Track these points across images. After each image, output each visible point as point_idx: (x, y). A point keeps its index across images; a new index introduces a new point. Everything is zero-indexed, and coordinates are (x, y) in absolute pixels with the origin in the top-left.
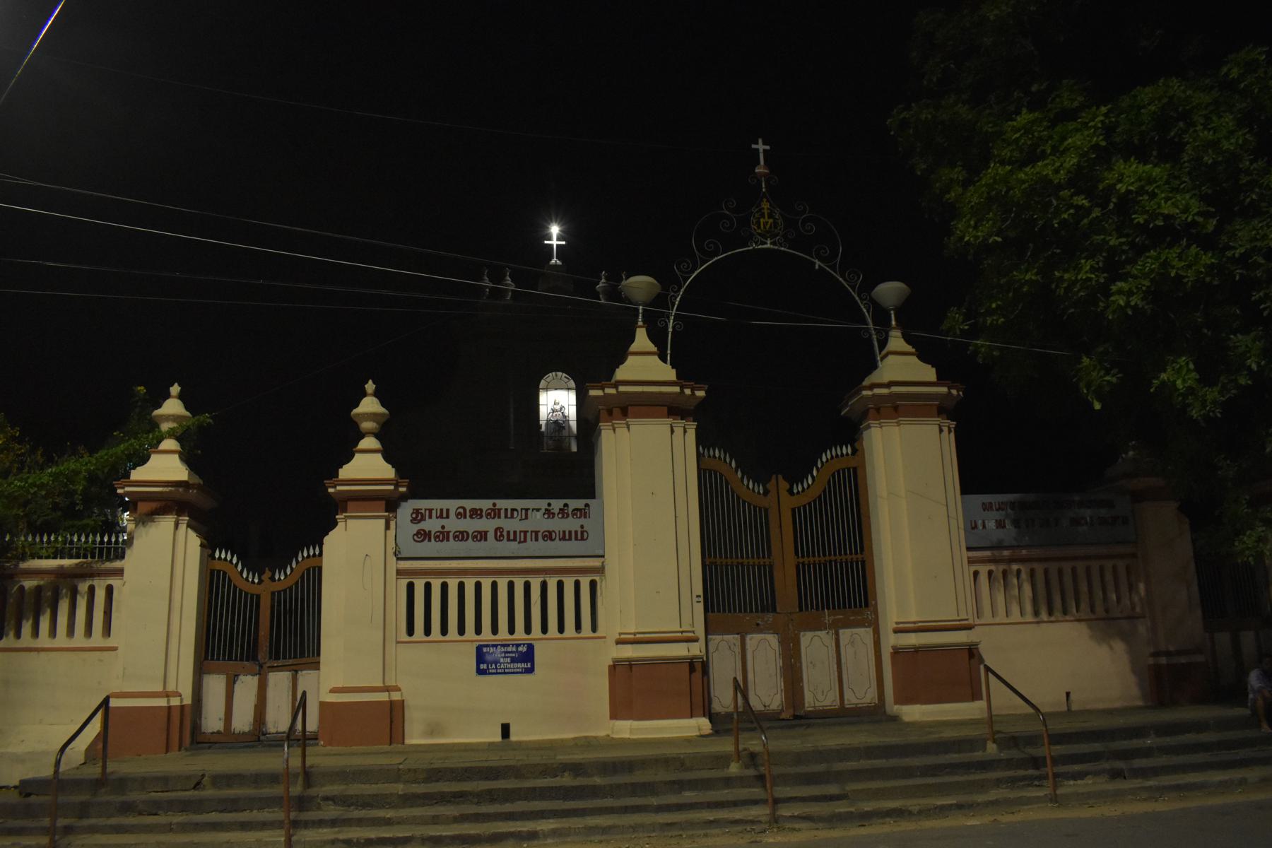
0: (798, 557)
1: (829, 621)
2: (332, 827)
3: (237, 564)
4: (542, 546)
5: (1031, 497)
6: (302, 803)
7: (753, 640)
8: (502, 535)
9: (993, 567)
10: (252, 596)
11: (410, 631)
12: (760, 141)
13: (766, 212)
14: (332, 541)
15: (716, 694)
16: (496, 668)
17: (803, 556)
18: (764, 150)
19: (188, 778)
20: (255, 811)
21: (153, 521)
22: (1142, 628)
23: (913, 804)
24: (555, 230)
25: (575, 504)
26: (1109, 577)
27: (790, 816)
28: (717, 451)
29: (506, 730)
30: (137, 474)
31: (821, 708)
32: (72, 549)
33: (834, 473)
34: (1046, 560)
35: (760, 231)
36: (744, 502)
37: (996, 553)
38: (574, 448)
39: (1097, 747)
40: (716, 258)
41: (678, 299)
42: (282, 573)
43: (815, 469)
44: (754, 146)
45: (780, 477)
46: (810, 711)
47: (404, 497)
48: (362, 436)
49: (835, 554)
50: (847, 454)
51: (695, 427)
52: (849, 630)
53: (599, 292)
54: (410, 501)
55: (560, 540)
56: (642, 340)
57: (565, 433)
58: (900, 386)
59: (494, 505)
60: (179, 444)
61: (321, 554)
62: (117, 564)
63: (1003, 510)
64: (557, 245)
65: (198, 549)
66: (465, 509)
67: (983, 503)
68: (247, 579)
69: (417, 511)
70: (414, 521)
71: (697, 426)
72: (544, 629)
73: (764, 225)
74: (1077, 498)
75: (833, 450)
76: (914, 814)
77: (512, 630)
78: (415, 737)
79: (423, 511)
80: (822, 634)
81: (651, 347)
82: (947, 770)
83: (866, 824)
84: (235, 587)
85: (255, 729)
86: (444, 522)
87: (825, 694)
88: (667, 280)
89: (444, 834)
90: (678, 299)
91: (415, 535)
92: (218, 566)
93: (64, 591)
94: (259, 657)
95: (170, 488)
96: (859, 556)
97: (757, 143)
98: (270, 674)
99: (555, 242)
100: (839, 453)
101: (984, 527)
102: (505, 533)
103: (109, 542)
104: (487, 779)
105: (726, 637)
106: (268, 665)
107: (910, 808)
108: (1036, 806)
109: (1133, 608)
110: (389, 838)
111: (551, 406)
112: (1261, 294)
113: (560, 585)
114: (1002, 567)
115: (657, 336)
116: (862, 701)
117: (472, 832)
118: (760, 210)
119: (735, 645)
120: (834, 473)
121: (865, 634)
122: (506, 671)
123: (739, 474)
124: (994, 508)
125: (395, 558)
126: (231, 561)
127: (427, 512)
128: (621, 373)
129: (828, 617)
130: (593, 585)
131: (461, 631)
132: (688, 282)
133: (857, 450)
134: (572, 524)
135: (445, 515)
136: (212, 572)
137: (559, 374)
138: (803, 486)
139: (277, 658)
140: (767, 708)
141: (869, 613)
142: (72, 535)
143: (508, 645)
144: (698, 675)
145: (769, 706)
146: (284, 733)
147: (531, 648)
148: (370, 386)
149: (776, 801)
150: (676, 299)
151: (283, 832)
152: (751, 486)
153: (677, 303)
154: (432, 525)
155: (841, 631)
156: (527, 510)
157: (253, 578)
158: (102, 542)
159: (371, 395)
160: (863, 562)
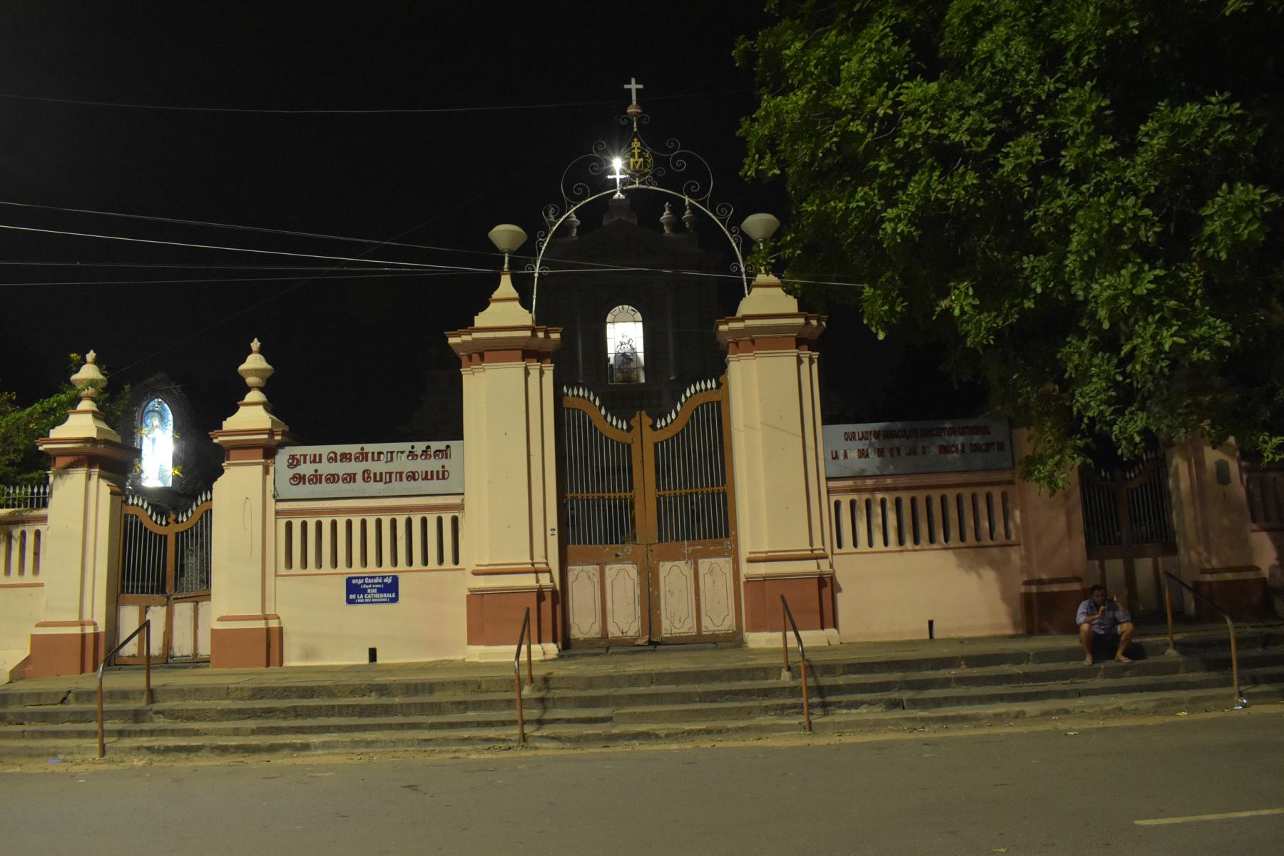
0: (659, 490)
2: (151, 736)
5: (898, 425)
6: (137, 716)
7: (612, 570)
8: (369, 477)
9: (855, 496)
10: (161, 536)
11: (289, 563)
12: (633, 80)
14: (220, 485)
16: (364, 598)
18: (637, 90)
19: (56, 694)
21: (68, 474)
23: (661, 728)
24: (617, 163)
25: (440, 445)
26: (982, 505)
28: (581, 390)
29: (373, 654)
30: (55, 433)
32: (8, 499)
34: (895, 489)
36: (607, 438)
37: (859, 482)
38: (643, 380)
39: (896, 676)
40: (584, 202)
41: (545, 245)
44: (626, 86)
45: (644, 413)
46: (666, 638)
47: (282, 445)
49: (697, 487)
50: (712, 388)
51: (552, 368)
52: (709, 560)
53: (663, 224)
54: (286, 448)
56: (506, 287)
57: (633, 365)
59: (362, 449)
61: (211, 499)
62: (42, 512)
63: (867, 439)
64: (621, 179)
65: (109, 496)
68: (156, 522)
69: (293, 457)
70: (291, 466)
71: (554, 367)
72: (410, 562)
74: (947, 425)
75: (703, 383)
76: (661, 738)
77: (380, 563)
78: (292, 660)
79: (298, 457)
80: (682, 563)
81: (515, 294)
82: (727, 696)
87: (682, 620)
88: (533, 226)
89: (230, 744)
90: (545, 245)
92: (130, 511)
94: (167, 590)
95: (80, 445)
96: (721, 488)
97: (630, 83)
99: (618, 177)
100: (703, 387)
101: (846, 456)
102: (372, 475)
103: (39, 493)
104: (304, 697)
106: (173, 597)
108: (788, 733)
109: (1008, 536)
111: (619, 339)
112: (1031, 213)
114: (865, 496)
115: (521, 285)
116: (720, 628)
117: (254, 743)
121: (724, 564)
122: (373, 600)
123: (603, 412)
125: (273, 501)
126: (142, 506)
127: (302, 457)
128: (481, 320)
129: (687, 547)
130: (455, 521)
131: (335, 563)
133: (722, 384)
134: (434, 465)
135: (317, 460)
136: (126, 516)
137: (626, 307)
138: (666, 421)
142: (9, 487)
143: (374, 577)
146: (188, 656)
147: (395, 579)
148: (255, 344)
151: (97, 740)
152: (614, 423)
153: (544, 248)
154: (306, 469)
155: (700, 561)
156: (392, 453)
157: (161, 521)
158: (33, 493)
159: (256, 352)
160: (725, 494)
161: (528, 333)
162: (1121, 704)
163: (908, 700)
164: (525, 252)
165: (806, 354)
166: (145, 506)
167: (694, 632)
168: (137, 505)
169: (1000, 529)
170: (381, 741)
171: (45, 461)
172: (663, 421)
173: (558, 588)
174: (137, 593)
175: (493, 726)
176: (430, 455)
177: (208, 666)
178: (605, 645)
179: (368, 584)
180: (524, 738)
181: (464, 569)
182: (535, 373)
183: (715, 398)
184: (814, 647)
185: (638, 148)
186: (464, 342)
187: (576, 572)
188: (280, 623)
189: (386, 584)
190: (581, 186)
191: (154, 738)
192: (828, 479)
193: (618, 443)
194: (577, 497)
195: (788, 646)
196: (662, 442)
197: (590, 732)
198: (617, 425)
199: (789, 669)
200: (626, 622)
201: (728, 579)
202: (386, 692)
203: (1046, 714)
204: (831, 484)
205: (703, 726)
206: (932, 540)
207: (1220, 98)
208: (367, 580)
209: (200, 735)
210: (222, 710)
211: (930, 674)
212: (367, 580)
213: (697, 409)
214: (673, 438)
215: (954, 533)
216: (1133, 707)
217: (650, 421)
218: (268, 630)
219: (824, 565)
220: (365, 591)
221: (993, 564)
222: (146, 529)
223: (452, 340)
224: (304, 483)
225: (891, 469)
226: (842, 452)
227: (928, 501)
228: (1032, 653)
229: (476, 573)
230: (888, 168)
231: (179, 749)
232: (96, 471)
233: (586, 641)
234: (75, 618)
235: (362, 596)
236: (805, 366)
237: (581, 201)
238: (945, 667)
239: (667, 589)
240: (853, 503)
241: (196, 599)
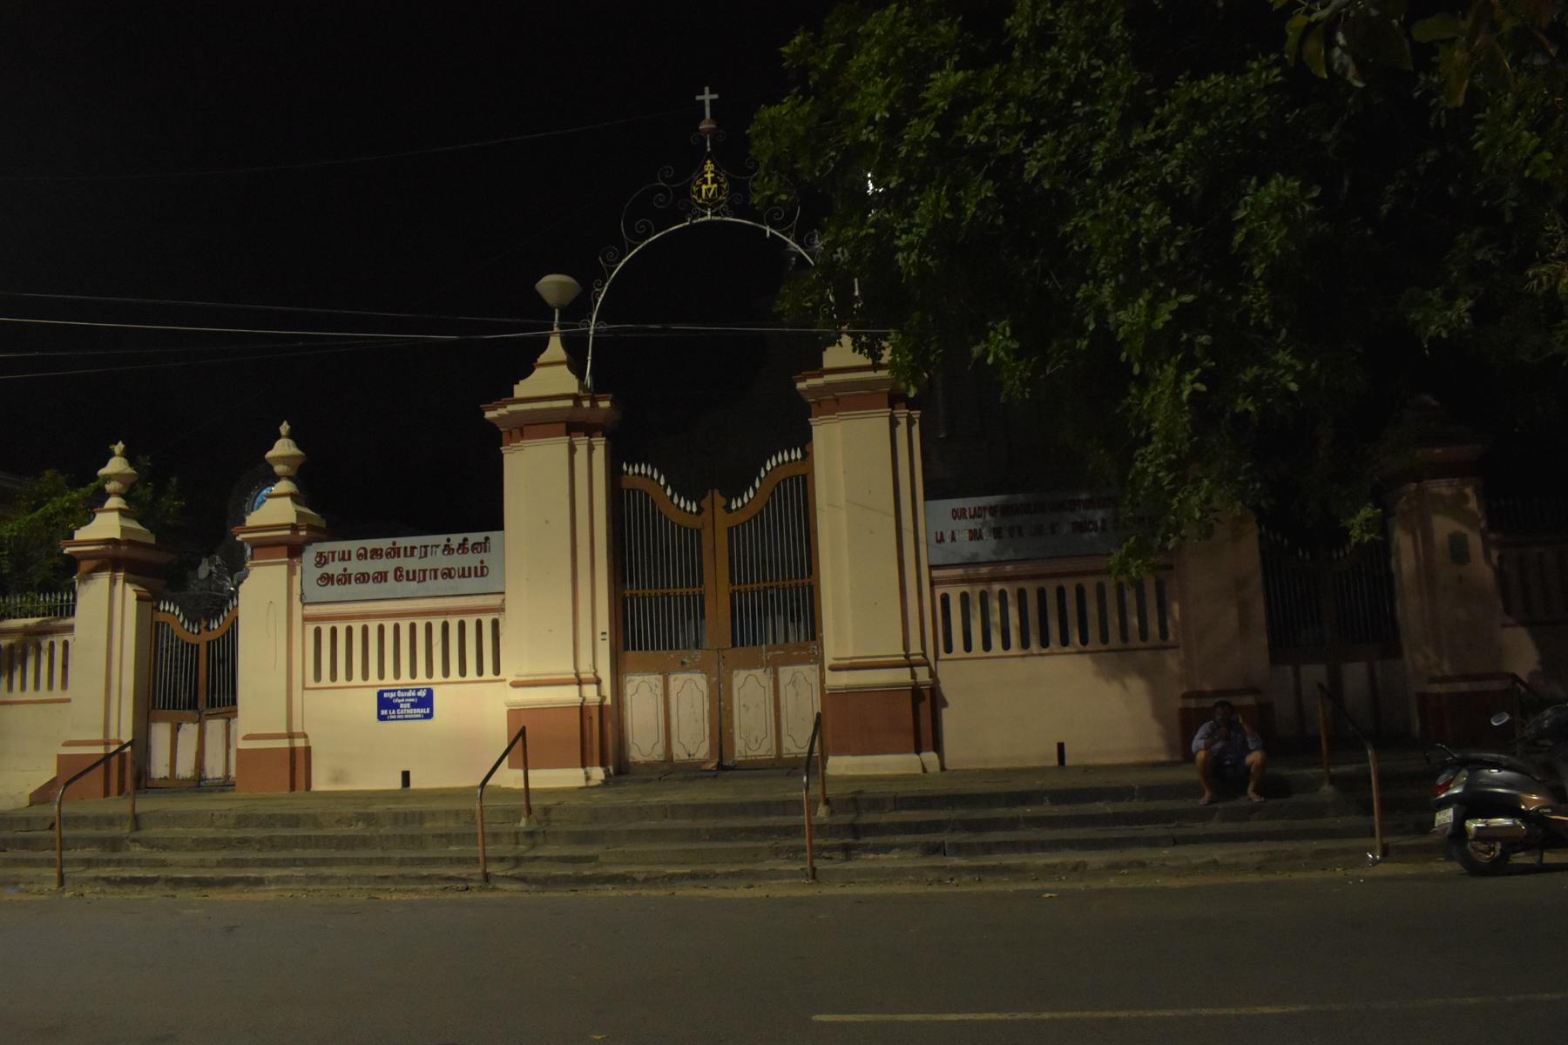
0: (733, 584)
1: (766, 657)
3: (179, 616)
4: (442, 584)
5: (1020, 498)
6: (115, 844)
7: (677, 680)
8: (401, 575)
9: (966, 588)
11: (318, 676)
12: (707, 89)
13: (709, 176)
15: (635, 741)
16: (396, 714)
17: (739, 583)
18: (711, 101)
19: (45, 819)
20: (79, 850)
21: (92, 579)
22: (1172, 661)
25: (475, 537)
27: (503, 876)
29: (406, 776)
30: (81, 534)
31: (753, 758)
33: (780, 483)
35: (700, 201)
37: (971, 571)
40: (646, 242)
41: (602, 296)
42: (216, 622)
43: (757, 480)
44: (699, 98)
45: (716, 492)
46: (739, 762)
47: (309, 542)
48: (276, 479)
50: (796, 459)
51: (603, 443)
54: (314, 544)
55: (459, 577)
56: (555, 349)
58: (536, 402)
59: (394, 543)
60: (294, 485)
61: (237, 606)
62: (69, 621)
63: (980, 516)
66: (365, 549)
67: (954, 510)
68: (188, 629)
69: (320, 555)
72: (446, 673)
73: (706, 193)
74: (1084, 496)
75: (786, 453)
78: (321, 783)
79: (326, 554)
80: (759, 672)
82: (743, 834)
83: (579, 889)
84: (183, 641)
85: (196, 775)
86: (346, 564)
87: (759, 741)
88: (587, 276)
90: (602, 296)
91: (318, 580)
92: (161, 617)
93: (31, 648)
94: (199, 706)
95: (102, 547)
96: (806, 580)
97: (703, 93)
98: (208, 721)
101: (953, 539)
102: (404, 573)
105: (647, 678)
106: (205, 713)
107: (634, 876)
108: (788, 881)
109: (1164, 634)
110: (140, 878)
113: (462, 625)
114: (979, 588)
116: (757, 753)
118: (702, 176)
119: (656, 686)
120: (780, 483)
121: (808, 672)
122: (406, 716)
123: (669, 492)
124: (968, 517)
125: (300, 604)
127: (330, 554)
128: (521, 390)
130: (495, 624)
131: (365, 676)
132: (614, 274)
134: (471, 560)
136: (157, 623)
139: (213, 706)
140: (692, 757)
141: (815, 647)
143: (407, 690)
144: (925, 708)
145: (694, 755)
146: (219, 779)
147: (430, 692)
148: (285, 428)
149: (487, 860)
150: (599, 296)
152: (682, 505)
153: (600, 300)
154: (335, 568)
155: (781, 669)
156: (426, 547)
158: (62, 601)
159: (118, 456)
160: (811, 588)
161: (570, 403)
162: (1217, 857)
163: (950, 844)
164: (576, 311)
165: (902, 414)
166: (177, 613)
167: (773, 754)
168: (169, 611)
169: (1154, 627)
170: (336, 877)
171: (71, 565)
172: (739, 500)
173: (608, 701)
174: (228, 705)
175: (466, 863)
176: (468, 549)
177: (234, 790)
178: (669, 770)
179: (400, 698)
180: (487, 877)
181: (505, 680)
182: (582, 450)
183: (801, 471)
184: (903, 775)
185: (712, 172)
186: (502, 417)
187: (636, 683)
188: (307, 742)
189: (419, 698)
190: (641, 224)
191: (120, 868)
192: (931, 567)
193: (686, 529)
194: (637, 594)
195: (531, 786)
196: (737, 527)
197: (559, 873)
198: (685, 507)
199: (827, 802)
200: (693, 742)
201: (814, 690)
202: (374, 821)
203: (1113, 868)
204: (935, 573)
205: (687, 870)
206: (1065, 641)
207: (1264, 61)
208: (400, 694)
209: (166, 866)
210: (197, 839)
211: (1000, 812)
212: (400, 694)
213: (778, 485)
214: (743, 524)
215: (1093, 632)
216: (1233, 860)
217: (723, 501)
218: (293, 750)
219: (923, 675)
220: (397, 706)
221: (1142, 672)
222: (178, 639)
223: (489, 415)
224: (333, 584)
225: (1010, 554)
226: (949, 533)
227: (1061, 592)
228: (1137, 788)
229: (515, 685)
230: (898, 184)
231: (135, 881)
232: (121, 575)
233: (647, 764)
234: (283, 730)
235: (394, 711)
236: (902, 431)
237: (644, 241)
238: (1023, 803)
239: (742, 703)
240: (965, 598)
241: (227, 715)
